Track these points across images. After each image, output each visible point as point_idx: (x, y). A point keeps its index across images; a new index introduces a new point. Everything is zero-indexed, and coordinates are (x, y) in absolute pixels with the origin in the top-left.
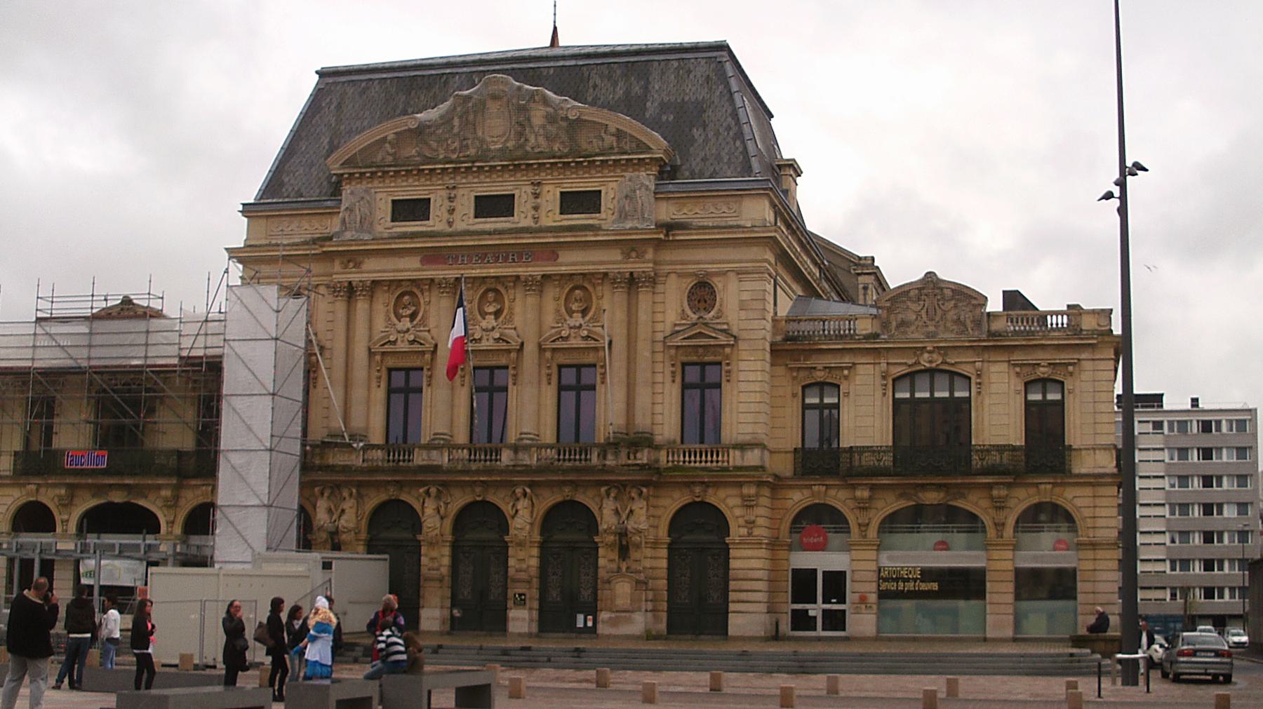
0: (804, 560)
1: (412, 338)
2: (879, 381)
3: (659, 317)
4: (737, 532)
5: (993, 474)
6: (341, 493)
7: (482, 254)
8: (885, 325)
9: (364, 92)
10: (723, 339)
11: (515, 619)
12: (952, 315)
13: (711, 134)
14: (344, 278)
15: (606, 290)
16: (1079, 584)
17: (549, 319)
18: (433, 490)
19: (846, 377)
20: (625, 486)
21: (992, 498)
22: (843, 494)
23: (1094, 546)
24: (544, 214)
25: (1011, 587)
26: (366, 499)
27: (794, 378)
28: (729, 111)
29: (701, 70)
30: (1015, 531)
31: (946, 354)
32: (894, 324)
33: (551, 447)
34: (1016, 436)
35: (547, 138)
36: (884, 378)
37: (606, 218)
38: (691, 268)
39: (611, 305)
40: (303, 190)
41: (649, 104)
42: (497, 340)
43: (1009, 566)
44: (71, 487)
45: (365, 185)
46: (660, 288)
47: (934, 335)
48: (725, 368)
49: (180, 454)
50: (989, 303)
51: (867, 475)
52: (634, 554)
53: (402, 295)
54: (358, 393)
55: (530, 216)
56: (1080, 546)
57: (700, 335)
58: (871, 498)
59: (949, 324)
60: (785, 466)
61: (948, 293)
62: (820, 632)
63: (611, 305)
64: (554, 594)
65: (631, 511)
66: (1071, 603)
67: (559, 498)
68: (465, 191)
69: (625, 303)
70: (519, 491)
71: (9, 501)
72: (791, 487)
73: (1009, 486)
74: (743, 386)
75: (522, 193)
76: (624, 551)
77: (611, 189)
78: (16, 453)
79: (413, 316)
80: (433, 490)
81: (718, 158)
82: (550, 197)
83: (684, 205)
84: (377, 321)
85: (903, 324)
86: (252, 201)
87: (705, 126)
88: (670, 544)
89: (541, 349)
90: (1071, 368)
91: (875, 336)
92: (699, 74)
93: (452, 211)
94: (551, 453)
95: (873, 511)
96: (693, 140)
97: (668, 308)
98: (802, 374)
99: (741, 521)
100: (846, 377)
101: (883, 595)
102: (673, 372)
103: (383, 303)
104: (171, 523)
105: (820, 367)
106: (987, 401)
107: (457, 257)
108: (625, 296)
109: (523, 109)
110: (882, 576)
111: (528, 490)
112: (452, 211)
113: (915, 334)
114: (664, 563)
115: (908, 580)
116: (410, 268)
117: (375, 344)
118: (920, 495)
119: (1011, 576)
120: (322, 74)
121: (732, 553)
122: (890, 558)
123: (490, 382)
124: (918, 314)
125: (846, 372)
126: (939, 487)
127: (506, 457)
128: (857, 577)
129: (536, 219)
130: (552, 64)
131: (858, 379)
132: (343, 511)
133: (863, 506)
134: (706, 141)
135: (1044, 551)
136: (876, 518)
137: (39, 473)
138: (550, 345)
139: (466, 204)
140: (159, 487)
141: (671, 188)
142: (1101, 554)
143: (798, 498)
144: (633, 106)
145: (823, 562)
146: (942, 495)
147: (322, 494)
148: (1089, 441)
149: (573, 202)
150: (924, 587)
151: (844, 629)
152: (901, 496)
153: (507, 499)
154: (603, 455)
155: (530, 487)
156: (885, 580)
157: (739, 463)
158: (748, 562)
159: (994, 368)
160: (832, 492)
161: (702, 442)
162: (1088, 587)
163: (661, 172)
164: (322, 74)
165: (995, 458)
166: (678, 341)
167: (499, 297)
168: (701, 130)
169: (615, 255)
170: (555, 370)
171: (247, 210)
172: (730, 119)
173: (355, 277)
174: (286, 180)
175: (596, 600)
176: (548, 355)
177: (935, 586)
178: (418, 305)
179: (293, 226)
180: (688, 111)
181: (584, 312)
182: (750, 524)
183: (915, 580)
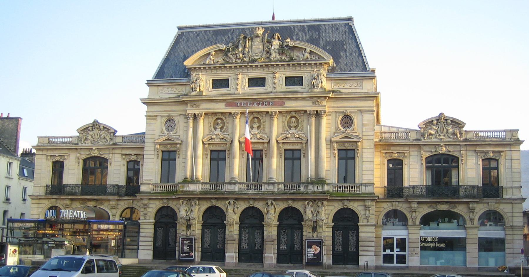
0: (387, 233)
4: (362, 222)
6: (191, 203)
10: (356, 140)
11: (268, 257)
18: (232, 202)
20: (315, 201)
21: (365, 206)
22: (405, 206)
23: (512, 228)
25: (477, 246)
26: (201, 205)
32: (426, 135)
33: (281, 183)
34: (122, 182)
35: (279, 54)
36: (79, 159)
38: (342, 109)
44: (72, 200)
48: (177, 153)
49: (119, 187)
50: (465, 126)
52: (319, 230)
55: (272, 86)
57: (346, 137)
59: (449, 135)
61: (102, 128)
62: (395, 264)
64: (283, 247)
65: (318, 211)
70: (269, 202)
71: (43, 206)
72: (382, 202)
76: (315, 229)
78: (47, 186)
79: (222, 128)
80: (232, 202)
81: (352, 64)
83: (338, 83)
87: (345, 51)
88: (240, 224)
91: (77, 144)
94: (207, 186)
95: (475, 213)
101: (422, 248)
107: (254, 103)
110: (422, 241)
112: (240, 85)
115: (432, 242)
116: (220, 108)
118: (438, 206)
119: (477, 241)
120: (179, 28)
121: (361, 230)
122: (425, 233)
123: (257, 157)
126: (447, 203)
127: (264, 188)
128: (411, 241)
133: (413, 211)
134: (346, 56)
135: (491, 232)
137: (57, 194)
140: (109, 200)
141: (333, 76)
142: (515, 232)
143: (386, 207)
145: (397, 233)
147: (183, 203)
148: (509, 185)
149: (291, 81)
150: (439, 245)
151: (405, 263)
152: (430, 206)
154: (307, 187)
155: (274, 200)
156: (423, 242)
161: (168, 182)
162: (510, 246)
164: (179, 28)
167: (259, 121)
169: (309, 103)
171: (149, 83)
173: (197, 112)
174: (166, 71)
175: (262, 249)
177: (444, 245)
178: (223, 123)
179: (164, 90)
180: (336, 43)
182: (367, 217)
183: (436, 242)
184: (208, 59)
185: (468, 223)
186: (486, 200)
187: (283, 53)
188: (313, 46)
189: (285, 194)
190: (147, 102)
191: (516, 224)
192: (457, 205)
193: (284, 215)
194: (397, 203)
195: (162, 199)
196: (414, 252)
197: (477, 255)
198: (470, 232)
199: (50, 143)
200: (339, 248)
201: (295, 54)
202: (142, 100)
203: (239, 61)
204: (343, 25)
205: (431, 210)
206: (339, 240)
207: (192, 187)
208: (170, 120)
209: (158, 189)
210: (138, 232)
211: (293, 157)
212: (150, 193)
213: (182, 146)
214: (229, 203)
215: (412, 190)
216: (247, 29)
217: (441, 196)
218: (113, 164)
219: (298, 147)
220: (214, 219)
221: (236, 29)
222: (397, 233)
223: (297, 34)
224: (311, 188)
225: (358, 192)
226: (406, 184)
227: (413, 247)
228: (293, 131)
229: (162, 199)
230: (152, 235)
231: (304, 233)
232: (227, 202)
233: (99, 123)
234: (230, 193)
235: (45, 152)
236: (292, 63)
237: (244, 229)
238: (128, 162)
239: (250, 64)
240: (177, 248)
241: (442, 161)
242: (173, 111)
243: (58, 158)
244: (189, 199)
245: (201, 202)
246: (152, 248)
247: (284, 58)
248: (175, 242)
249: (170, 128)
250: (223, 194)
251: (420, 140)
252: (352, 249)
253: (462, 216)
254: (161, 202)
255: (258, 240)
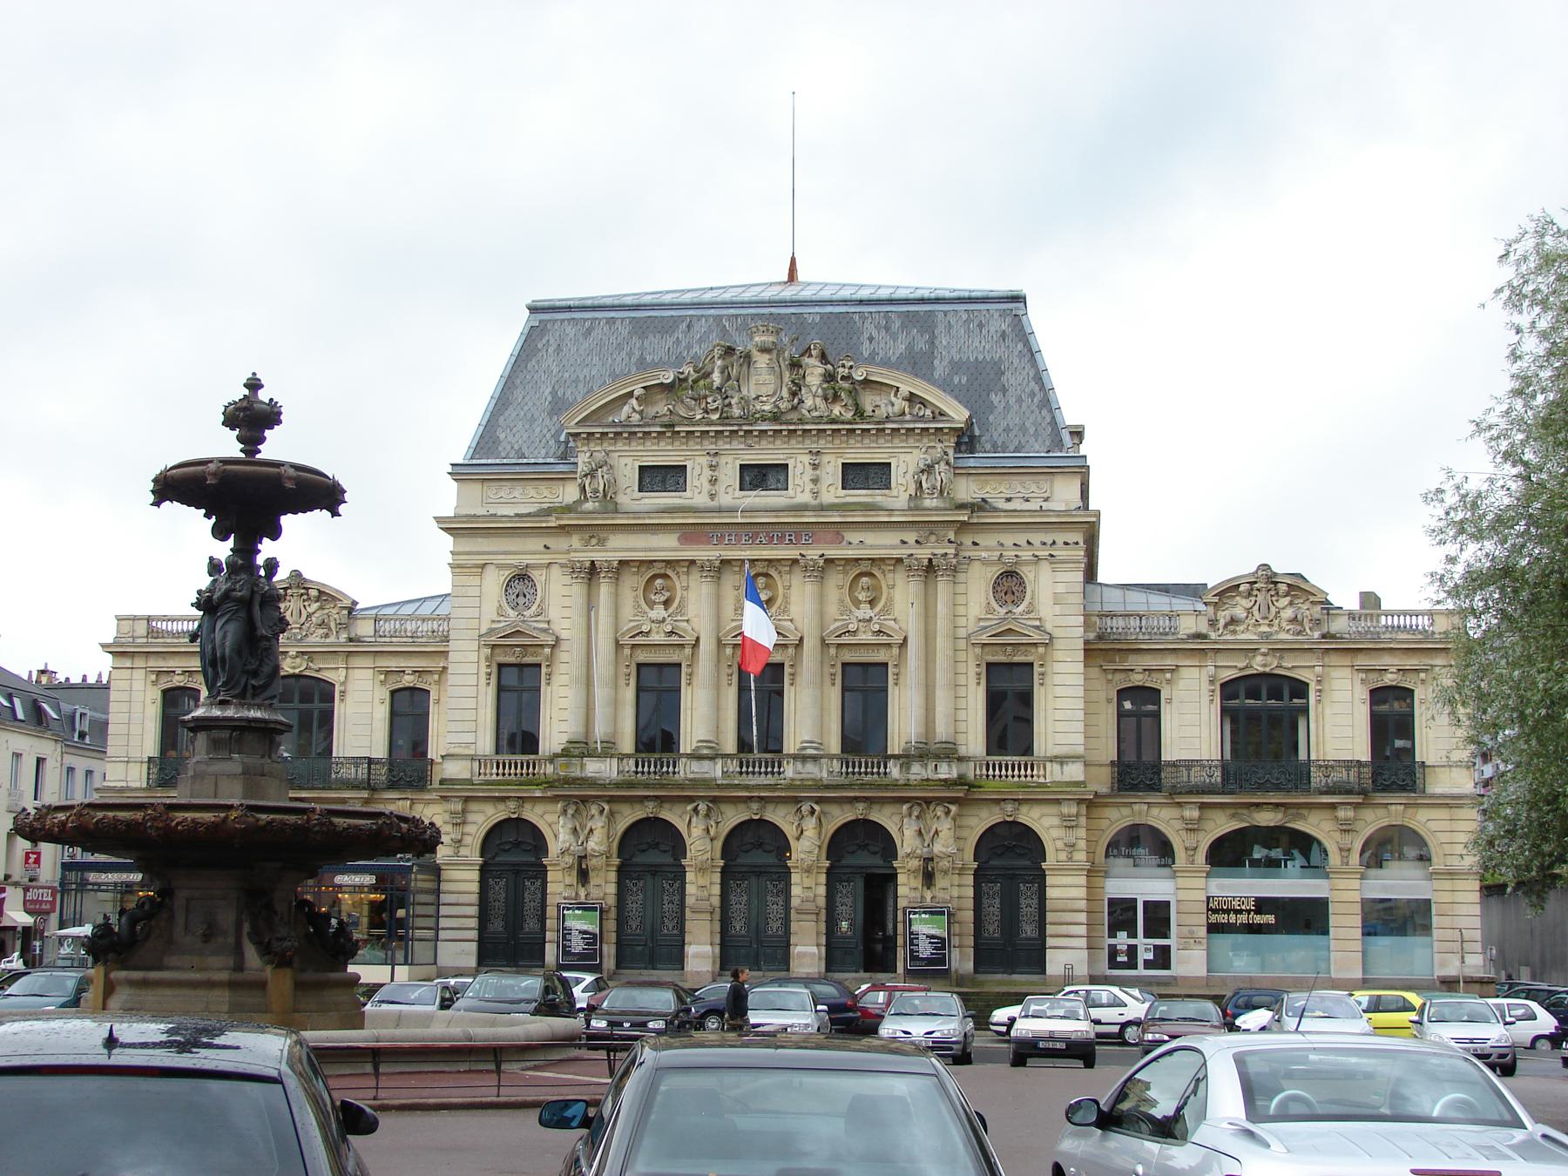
1: (669, 628)
2: (1206, 686)
3: (961, 610)
5: (1340, 793)
7: (753, 531)
8: (1213, 623)
9: (589, 332)
10: (1036, 637)
11: (802, 955)
12: (1288, 613)
13: (1012, 401)
14: (587, 556)
15: (899, 577)
16: (1434, 919)
17: (832, 610)
18: (702, 807)
19: (1169, 681)
23: (1451, 874)
24: (723, 489)
27: (1109, 681)
28: (1032, 374)
29: (998, 325)
30: (1107, 856)
31: (1281, 658)
37: (898, 494)
39: (903, 595)
40: (524, 449)
41: (936, 362)
42: (672, 633)
43: (1356, 896)
45: (607, 446)
46: (961, 577)
47: (1267, 635)
49: (370, 761)
51: (1198, 793)
52: (940, 881)
53: (655, 577)
54: (601, 694)
55: (807, 490)
56: (1432, 876)
58: (1200, 819)
59: (1284, 624)
60: (1102, 782)
63: (903, 595)
66: (1426, 939)
67: (744, 817)
68: (730, 459)
69: (585, 591)
72: (1106, 805)
73: (1357, 806)
74: (1059, 691)
75: (799, 465)
76: (928, 878)
77: (905, 462)
80: (702, 807)
81: (1023, 429)
82: (830, 468)
83: (987, 482)
84: (623, 607)
85: (1233, 621)
86: (461, 461)
87: (1004, 390)
88: (976, 870)
89: (824, 644)
90: (1422, 675)
92: (992, 330)
93: (712, 483)
96: (992, 408)
97: (974, 596)
98: (1118, 676)
99: (1060, 844)
100: (1169, 681)
101: (1213, 929)
102: (978, 674)
103: (632, 583)
104: (1345, 851)
105: (1139, 669)
106: (1328, 712)
108: (922, 586)
109: (795, 365)
110: (1213, 907)
111: (816, 807)
112: (712, 483)
113: (1245, 635)
114: (970, 892)
115: (1240, 912)
116: (665, 546)
117: (726, 635)
119: (1357, 908)
120: (534, 309)
121: (1049, 880)
122: (1221, 887)
123: (762, 687)
124: (1249, 611)
125: (1168, 676)
127: (790, 770)
128: (1183, 908)
129: (816, 494)
130: (817, 309)
131: (1182, 684)
132: (591, 830)
133: (1192, 828)
134: (1007, 408)
135: (1398, 882)
136: (1205, 841)
138: (832, 640)
139: (730, 474)
141: (972, 463)
142: (1460, 885)
143: (1117, 818)
144: (918, 364)
145: (1143, 885)
146: (1280, 816)
149: (855, 474)
150: (1259, 919)
152: (1233, 816)
153: (790, 818)
154: (905, 767)
157: (1058, 778)
158: (1065, 889)
159: (1335, 673)
160: (1155, 811)
162: (1446, 921)
163: (958, 444)
164: (534, 309)
165: (1339, 776)
166: (984, 638)
168: (1000, 395)
170: (495, 669)
171: (460, 473)
172: (1032, 384)
173: (598, 556)
174: (502, 436)
176: (833, 651)
177: (1271, 919)
178: (671, 589)
179: (516, 494)
181: (872, 603)
183: (1249, 912)
184: (626, 408)
185: (1334, 859)
186: (1380, 798)
187: (836, 398)
188: (918, 381)
189: (850, 786)
190: (455, 527)
191: (1455, 862)
192: (1305, 812)
193: (842, 843)
194: (1145, 807)
195: (503, 799)
196: (1189, 940)
197: (1358, 946)
198: (1341, 884)
199: (152, 633)
200: (992, 929)
201: (868, 401)
202: (439, 520)
203: (715, 417)
204: (996, 315)
205: (1235, 825)
206: (993, 907)
207: (593, 768)
208: (521, 578)
209: (492, 774)
210: (437, 892)
211: (864, 686)
212: (470, 782)
213: (557, 651)
214: (695, 810)
215: (1185, 773)
216: (730, 317)
217: (1262, 787)
218: (349, 698)
219: (880, 656)
220: (649, 852)
221: (699, 318)
222: (1143, 885)
223: (871, 339)
224: (917, 771)
225: (1042, 780)
226: (1166, 756)
227: (1187, 923)
228: (865, 611)
229: (503, 799)
230: (474, 898)
231: (550, 888)
232: (690, 807)
233: (1275, 574)
234: (695, 783)
235: (140, 662)
236: (860, 425)
237: (841, 881)
238: (393, 693)
239: (742, 427)
240: (549, 936)
241: (1264, 693)
242: (527, 551)
243: (1140, 677)
244: (585, 800)
245: (616, 807)
246: (474, 934)
247: (837, 410)
248: (542, 919)
249: (521, 600)
250: (680, 786)
251: (1205, 637)
252: (1029, 930)
253: (1319, 843)
254: (501, 806)
255: (775, 909)
